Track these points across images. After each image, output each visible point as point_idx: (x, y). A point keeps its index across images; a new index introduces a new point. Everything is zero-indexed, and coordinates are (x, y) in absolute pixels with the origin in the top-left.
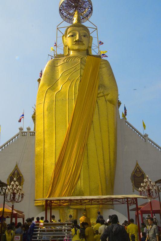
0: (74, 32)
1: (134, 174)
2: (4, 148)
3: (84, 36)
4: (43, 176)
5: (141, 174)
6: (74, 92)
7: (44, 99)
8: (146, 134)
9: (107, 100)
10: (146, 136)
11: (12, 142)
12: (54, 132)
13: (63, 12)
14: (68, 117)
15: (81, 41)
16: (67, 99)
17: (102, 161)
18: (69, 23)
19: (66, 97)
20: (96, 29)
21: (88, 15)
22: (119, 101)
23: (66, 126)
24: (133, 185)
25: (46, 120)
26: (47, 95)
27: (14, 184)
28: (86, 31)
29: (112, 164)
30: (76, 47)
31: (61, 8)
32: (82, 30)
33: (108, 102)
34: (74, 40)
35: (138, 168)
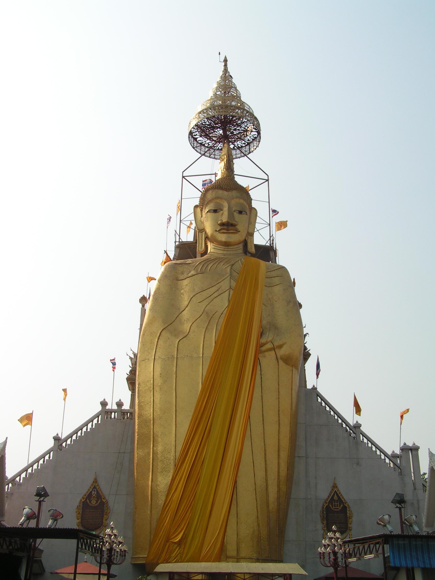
0: (218, 201)
1: (327, 506)
3: (240, 212)
5: (342, 506)
7: (154, 350)
8: (357, 422)
9: (279, 357)
10: (357, 426)
12: (174, 423)
15: (233, 225)
20: (267, 180)
22: (305, 348)
27: (110, 533)
29: (284, 488)
30: (222, 237)
31: (192, 130)
32: (237, 198)
33: (280, 361)
35: (337, 493)
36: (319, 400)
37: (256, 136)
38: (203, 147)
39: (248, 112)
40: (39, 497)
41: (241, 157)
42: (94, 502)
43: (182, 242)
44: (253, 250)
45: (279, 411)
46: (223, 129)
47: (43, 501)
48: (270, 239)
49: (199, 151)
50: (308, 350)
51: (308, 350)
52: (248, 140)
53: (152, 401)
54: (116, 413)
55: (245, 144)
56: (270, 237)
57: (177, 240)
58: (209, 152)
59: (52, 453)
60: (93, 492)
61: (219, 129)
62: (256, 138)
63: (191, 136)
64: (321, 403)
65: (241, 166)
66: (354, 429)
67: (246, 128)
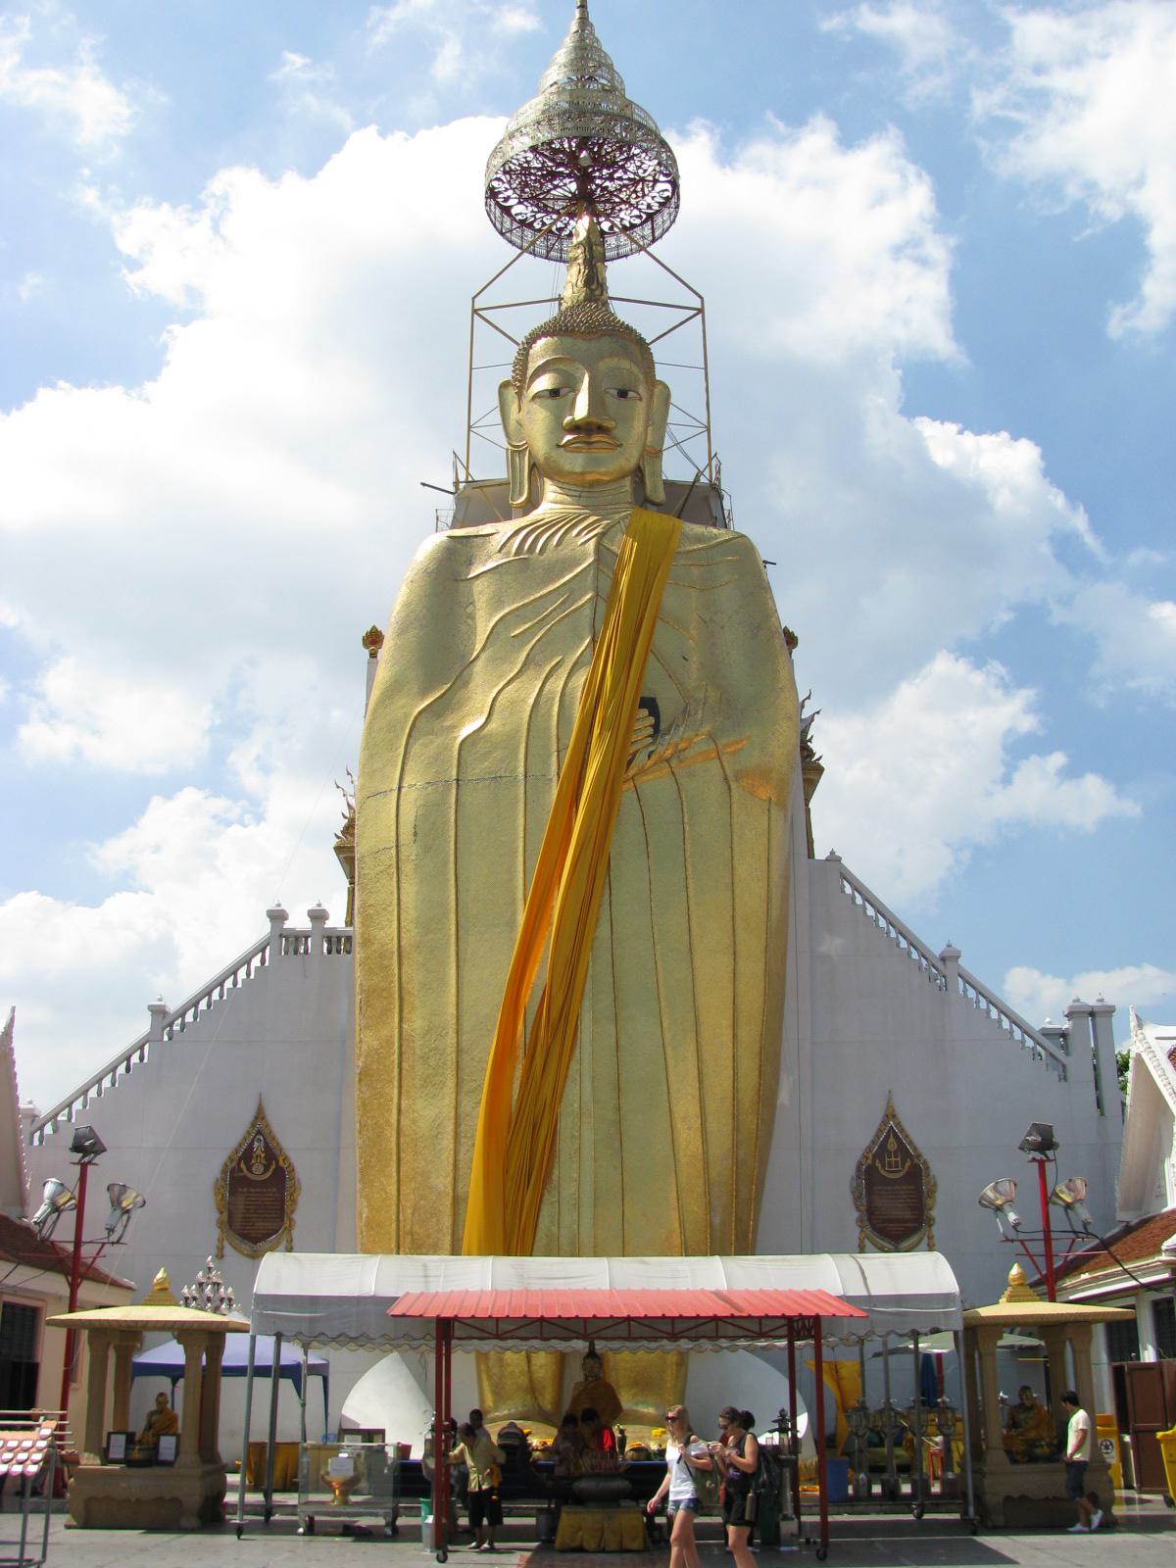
2: (195, 1018)
4: (395, 1179)
5: (908, 1164)
6: (554, 739)
11: (235, 983)
13: (507, 199)
14: (521, 875)
15: (601, 429)
16: (521, 777)
17: (695, 1109)
18: (546, 258)
19: (516, 768)
20: (701, 311)
21: (657, 212)
23: (512, 924)
24: (860, 1221)
25: (410, 889)
26: (417, 746)
28: (635, 362)
29: (749, 1121)
31: (495, 184)
32: (611, 355)
34: (568, 419)
36: (848, 889)
37: (669, 194)
38: (528, 233)
39: (641, 126)
40: (81, 1155)
41: (632, 252)
42: (258, 1168)
43: (474, 481)
44: (660, 496)
45: (733, 917)
46: (577, 179)
47: (90, 1162)
48: (710, 464)
49: (519, 241)
50: (816, 757)
51: (816, 757)
52: (649, 206)
53: (395, 901)
54: (310, 939)
55: (640, 217)
56: (710, 459)
57: (462, 478)
58: (549, 244)
59: (146, 1047)
60: (256, 1144)
61: (567, 180)
62: (668, 199)
63: (493, 203)
64: (853, 898)
65: (623, 276)
66: (940, 965)
67: (640, 171)
